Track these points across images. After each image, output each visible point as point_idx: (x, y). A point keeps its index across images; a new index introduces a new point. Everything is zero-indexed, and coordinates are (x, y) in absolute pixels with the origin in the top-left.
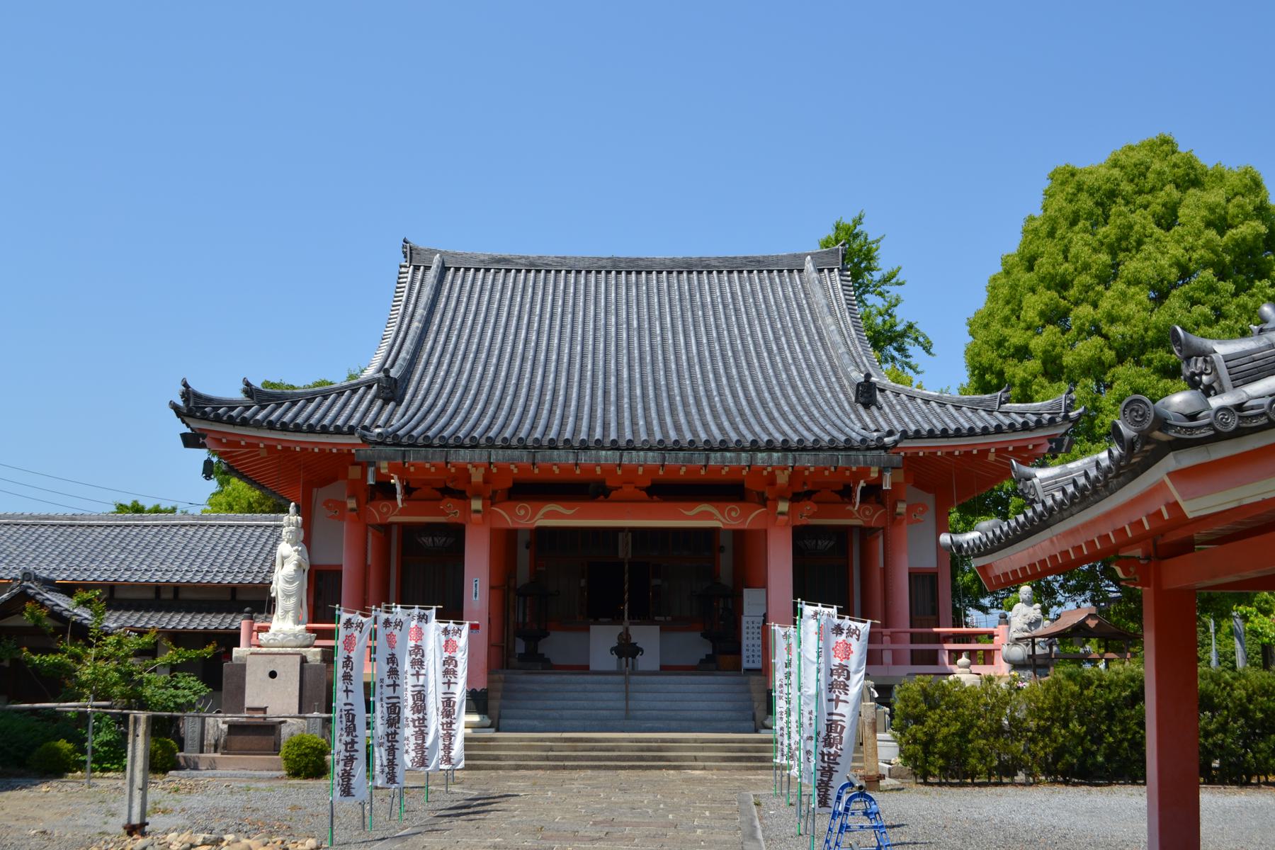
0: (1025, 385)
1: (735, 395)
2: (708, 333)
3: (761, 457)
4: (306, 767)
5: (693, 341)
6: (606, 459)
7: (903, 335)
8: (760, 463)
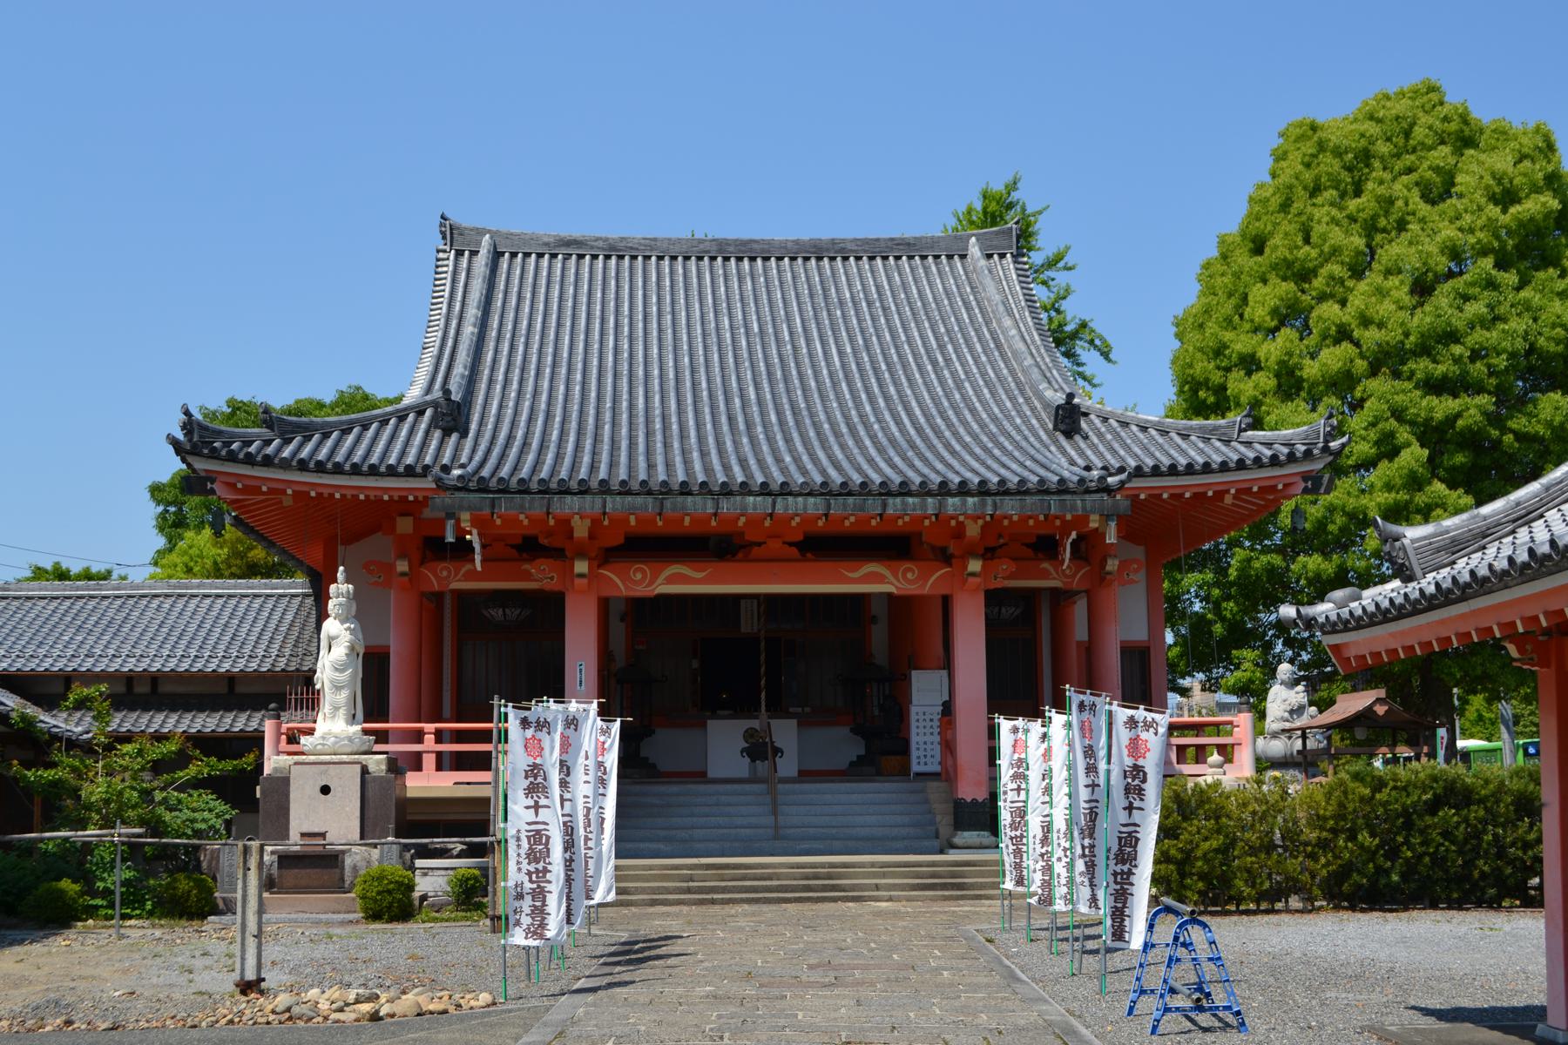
0: (1255, 404)
1: (899, 423)
2: (852, 340)
4: (390, 907)
5: (834, 351)
6: (755, 508)
7: (1074, 335)
8: (951, 511)
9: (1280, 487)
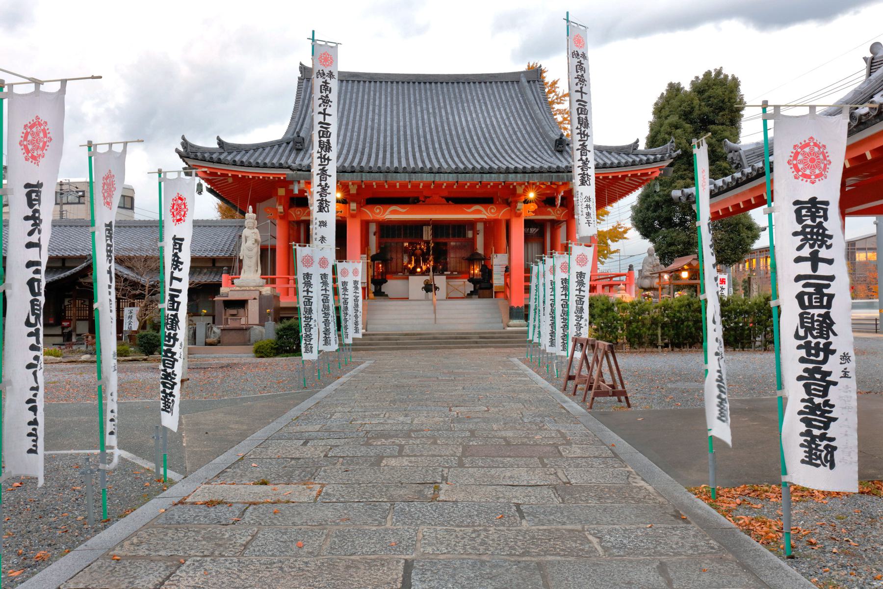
8: (510, 180)
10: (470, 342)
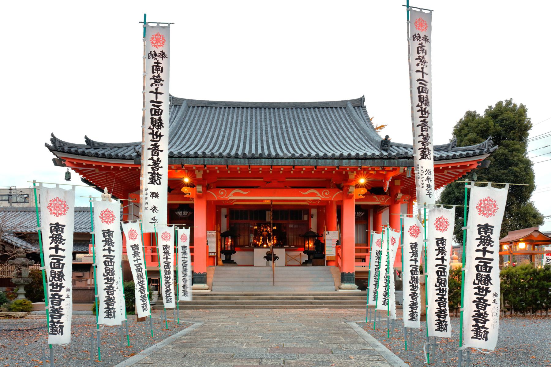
3: (345, 162)
9: (468, 165)
10: (305, 303)
